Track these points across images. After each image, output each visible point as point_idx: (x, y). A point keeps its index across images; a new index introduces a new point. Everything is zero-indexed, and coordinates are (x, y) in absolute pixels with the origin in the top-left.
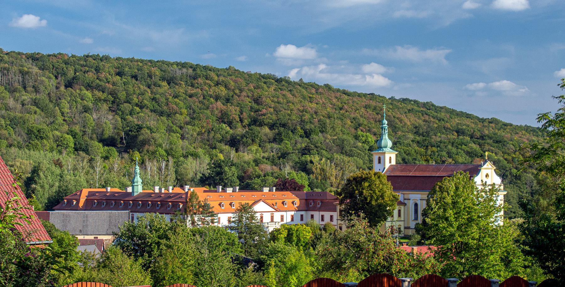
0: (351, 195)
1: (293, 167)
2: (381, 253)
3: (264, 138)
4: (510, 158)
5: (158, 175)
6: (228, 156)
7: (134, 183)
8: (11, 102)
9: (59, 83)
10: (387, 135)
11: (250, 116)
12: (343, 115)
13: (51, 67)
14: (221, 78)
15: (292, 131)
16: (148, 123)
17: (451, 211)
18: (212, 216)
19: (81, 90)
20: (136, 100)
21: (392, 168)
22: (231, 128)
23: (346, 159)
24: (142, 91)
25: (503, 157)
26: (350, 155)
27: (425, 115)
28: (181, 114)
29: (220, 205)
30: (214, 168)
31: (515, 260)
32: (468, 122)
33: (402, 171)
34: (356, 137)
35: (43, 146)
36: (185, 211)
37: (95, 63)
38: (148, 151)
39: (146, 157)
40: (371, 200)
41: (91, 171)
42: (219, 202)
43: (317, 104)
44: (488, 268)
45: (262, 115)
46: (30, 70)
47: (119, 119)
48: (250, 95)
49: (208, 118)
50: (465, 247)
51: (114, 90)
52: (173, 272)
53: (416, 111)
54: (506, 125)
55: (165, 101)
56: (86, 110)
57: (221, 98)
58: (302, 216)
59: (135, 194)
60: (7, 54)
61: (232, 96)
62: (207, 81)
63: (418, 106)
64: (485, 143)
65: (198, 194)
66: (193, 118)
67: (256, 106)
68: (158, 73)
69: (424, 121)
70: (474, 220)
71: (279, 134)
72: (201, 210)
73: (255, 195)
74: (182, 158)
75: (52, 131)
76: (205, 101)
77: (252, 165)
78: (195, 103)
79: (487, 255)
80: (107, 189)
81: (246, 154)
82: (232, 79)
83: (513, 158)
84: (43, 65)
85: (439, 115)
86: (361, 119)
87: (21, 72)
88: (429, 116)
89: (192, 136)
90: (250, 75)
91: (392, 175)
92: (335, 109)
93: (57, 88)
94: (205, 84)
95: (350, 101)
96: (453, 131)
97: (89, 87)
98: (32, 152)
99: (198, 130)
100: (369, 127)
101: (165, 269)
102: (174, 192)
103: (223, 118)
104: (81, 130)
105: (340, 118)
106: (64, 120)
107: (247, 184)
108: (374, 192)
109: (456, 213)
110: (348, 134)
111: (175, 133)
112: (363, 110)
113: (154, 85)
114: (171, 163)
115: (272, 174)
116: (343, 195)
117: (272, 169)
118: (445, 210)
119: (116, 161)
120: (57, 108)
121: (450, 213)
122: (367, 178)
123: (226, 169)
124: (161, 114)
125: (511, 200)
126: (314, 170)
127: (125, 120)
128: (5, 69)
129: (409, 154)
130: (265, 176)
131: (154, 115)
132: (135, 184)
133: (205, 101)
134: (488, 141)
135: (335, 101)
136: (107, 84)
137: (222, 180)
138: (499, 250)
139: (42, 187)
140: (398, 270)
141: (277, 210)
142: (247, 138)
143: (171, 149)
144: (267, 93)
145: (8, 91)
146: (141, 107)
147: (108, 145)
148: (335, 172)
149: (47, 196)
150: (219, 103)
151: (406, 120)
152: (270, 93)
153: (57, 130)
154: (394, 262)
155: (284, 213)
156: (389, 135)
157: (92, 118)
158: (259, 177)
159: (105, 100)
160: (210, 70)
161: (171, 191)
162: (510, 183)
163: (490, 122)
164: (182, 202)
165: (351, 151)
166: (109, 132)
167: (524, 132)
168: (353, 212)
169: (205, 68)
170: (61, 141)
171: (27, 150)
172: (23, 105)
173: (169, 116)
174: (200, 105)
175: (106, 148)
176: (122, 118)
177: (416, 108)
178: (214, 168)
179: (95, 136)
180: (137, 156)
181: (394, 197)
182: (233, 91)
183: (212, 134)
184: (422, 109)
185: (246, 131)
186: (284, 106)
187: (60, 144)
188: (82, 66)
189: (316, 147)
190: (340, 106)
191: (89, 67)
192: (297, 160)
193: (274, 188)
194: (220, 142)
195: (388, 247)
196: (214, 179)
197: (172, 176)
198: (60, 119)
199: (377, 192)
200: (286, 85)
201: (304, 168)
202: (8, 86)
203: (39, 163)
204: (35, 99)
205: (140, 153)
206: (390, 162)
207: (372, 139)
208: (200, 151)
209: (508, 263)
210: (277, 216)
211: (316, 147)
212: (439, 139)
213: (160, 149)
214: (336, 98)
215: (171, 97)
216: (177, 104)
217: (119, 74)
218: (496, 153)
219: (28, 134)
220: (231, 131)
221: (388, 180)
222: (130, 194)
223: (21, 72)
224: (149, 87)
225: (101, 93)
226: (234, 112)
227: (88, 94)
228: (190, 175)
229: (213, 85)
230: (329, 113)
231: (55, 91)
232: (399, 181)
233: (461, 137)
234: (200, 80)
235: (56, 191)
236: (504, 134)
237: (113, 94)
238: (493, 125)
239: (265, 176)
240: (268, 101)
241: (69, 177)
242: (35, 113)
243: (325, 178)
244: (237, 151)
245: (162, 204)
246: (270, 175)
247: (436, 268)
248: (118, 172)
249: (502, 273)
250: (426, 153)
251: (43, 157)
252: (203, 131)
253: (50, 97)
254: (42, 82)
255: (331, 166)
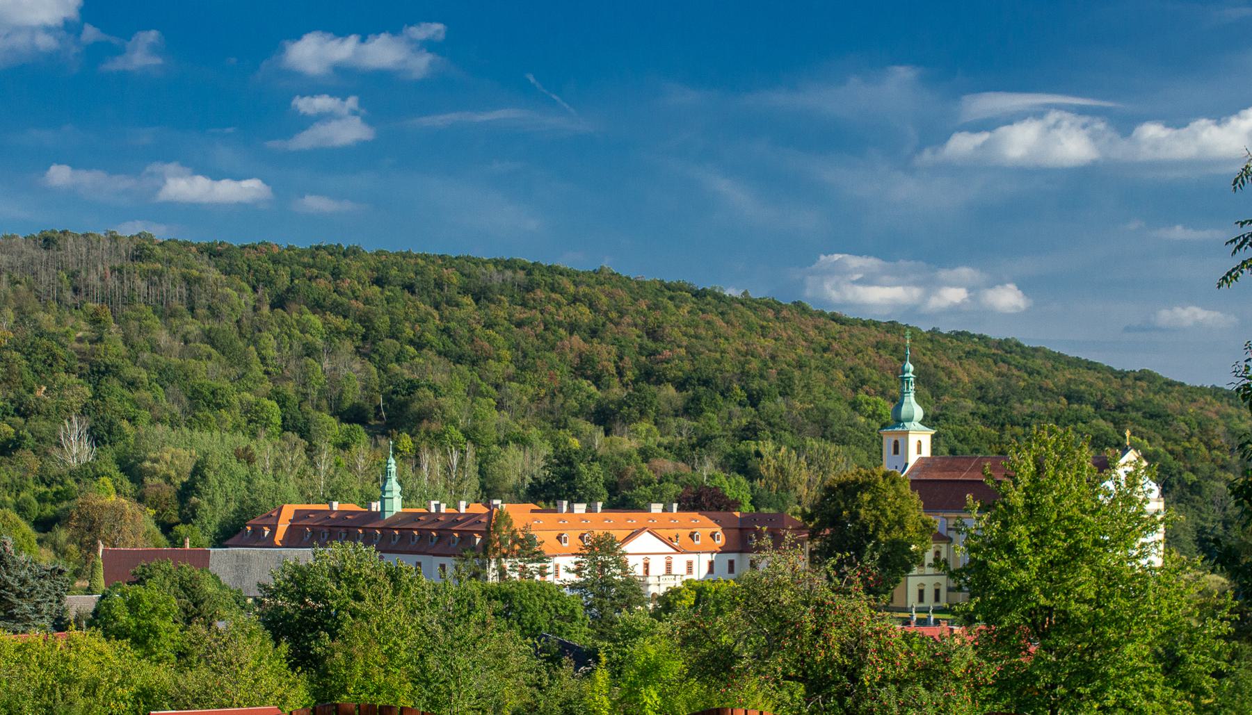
0: (834, 520)
1: (723, 466)
2: (834, 633)
3: (665, 407)
4: (1179, 449)
5: (443, 478)
6: (588, 445)
7: (384, 492)
8: (163, 337)
9: (259, 300)
10: (912, 394)
11: (637, 364)
12: (829, 362)
13: (246, 268)
14: (583, 289)
15: (722, 394)
16: (431, 377)
17: (1021, 528)
18: (540, 560)
19: (301, 313)
20: (409, 332)
21: (923, 464)
22: (598, 388)
23: (832, 448)
24: (422, 314)
25: (1164, 446)
26: (842, 442)
27: (1001, 364)
28: (499, 360)
29: (559, 538)
30: (558, 465)
31: (1192, 657)
32: (1090, 377)
33: (943, 470)
34: (855, 406)
35: (221, 422)
36: (486, 550)
37: (332, 261)
38: (427, 433)
39: (424, 444)
40: (876, 530)
41: (310, 471)
42: (556, 533)
43: (776, 340)
44: (1121, 677)
45: (662, 362)
46: (204, 275)
47: (374, 370)
48: (640, 322)
49: (552, 367)
50: (1067, 622)
51: (366, 314)
52: (365, 675)
53: (983, 355)
54: (1170, 384)
55: (467, 335)
56: (310, 351)
57: (580, 327)
58: (731, 563)
59: (388, 515)
60: (161, 244)
61: (604, 325)
62: (553, 295)
63: (987, 346)
64: (1126, 418)
65: (512, 515)
66: (523, 369)
67: (650, 344)
68: (455, 279)
69: (999, 374)
70: (1084, 549)
71: (696, 399)
72: (517, 547)
73: (634, 518)
74: (495, 447)
75: (239, 391)
76: (548, 335)
77: (636, 461)
78: (528, 339)
79: (1116, 643)
80: (331, 506)
81: (626, 438)
82: (603, 291)
83: (1186, 450)
84: (230, 265)
85: (1030, 364)
86: (867, 371)
87: (187, 280)
88: (1009, 364)
89: (518, 403)
90: (642, 285)
91: (923, 478)
92: (814, 350)
93: (255, 309)
94: (550, 300)
95: (845, 335)
96: (1058, 394)
97: (317, 306)
98: (196, 433)
99: (532, 391)
100: (882, 386)
101: (347, 668)
102: (469, 511)
103: (584, 368)
104: (297, 392)
105: (823, 368)
106: (266, 372)
107: (624, 498)
108: (883, 513)
109: (1036, 534)
110: (838, 399)
111: (484, 396)
112: (871, 351)
113: (448, 303)
114: (470, 456)
115: (676, 477)
116: (817, 520)
117: (676, 468)
118: (1005, 524)
119: (362, 452)
120: (252, 348)
121: (1021, 533)
122: (868, 484)
123: (582, 467)
124: (459, 359)
125: (1182, 536)
126: (763, 469)
127: (385, 371)
128: (155, 272)
129: (964, 440)
130: (660, 482)
131: (444, 361)
132: (388, 495)
133: (548, 335)
134: (1133, 414)
135: (812, 333)
136: (353, 302)
137: (572, 489)
138: (1151, 630)
139: (211, 502)
140: (877, 679)
141: (678, 551)
142: (630, 407)
143: (475, 429)
144: (673, 318)
145: (160, 317)
146: (419, 346)
147: (349, 421)
148: (803, 473)
149: (218, 520)
150: (576, 340)
151: (960, 373)
152: (681, 319)
153: (249, 390)
154: (869, 657)
155: (693, 557)
156: (917, 396)
157: (321, 368)
158: (648, 483)
159: (349, 334)
160: (561, 274)
161: (463, 510)
162: (1179, 501)
163: (1136, 379)
164: (480, 533)
165: (843, 432)
166: (353, 395)
167: (1209, 398)
168: (765, 528)
169: (552, 270)
170: (256, 412)
171: (186, 430)
172: (186, 342)
173: (474, 363)
174: (536, 343)
175: (345, 426)
176: (379, 368)
177: (982, 349)
178: (558, 465)
179: (324, 403)
180: (406, 441)
181: (925, 524)
182: (606, 314)
183: (560, 400)
184: (993, 351)
185: (629, 394)
186: (708, 343)
187: (253, 419)
188: (306, 266)
189: (770, 424)
190: (824, 343)
191: (319, 269)
192: (729, 450)
193: (675, 506)
194: (575, 415)
195: (852, 619)
196: (550, 491)
197: (474, 482)
198: (257, 370)
199: (889, 513)
200: (715, 302)
201: (743, 466)
202: (159, 307)
203: (206, 455)
204: (210, 331)
205: (412, 436)
206: (919, 451)
207: (886, 408)
208: (534, 433)
209: (1173, 665)
210: (679, 562)
211: (770, 424)
212: (1028, 411)
213: (452, 429)
214: (817, 327)
215: (479, 327)
216: (490, 340)
217: (379, 282)
218: (1149, 440)
219: (190, 398)
220: (599, 394)
221: (913, 489)
222: (379, 515)
223: (187, 280)
224: (437, 308)
225: (341, 319)
226: (605, 355)
227: (316, 320)
228: (512, 480)
229: (565, 302)
230: (800, 357)
231: (251, 314)
232: (937, 490)
233: (1076, 406)
234: (540, 294)
235: (236, 511)
236: (1171, 404)
237: (365, 320)
238: (1144, 384)
239: (660, 482)
240: (676, 333)
241: (262, 481)
242: (209, 357)
243: (785, 488)
244: (607, 433)
245: (439, 536)
246: (672, 479)
247: (979, 676)
248: (365, 473)
249: (1157, 691)
250: (1000, 437)
251: (216, 442)
252: (543, 391)
253: (239, 327)
254: (225, 299)
255: (798, 463)
